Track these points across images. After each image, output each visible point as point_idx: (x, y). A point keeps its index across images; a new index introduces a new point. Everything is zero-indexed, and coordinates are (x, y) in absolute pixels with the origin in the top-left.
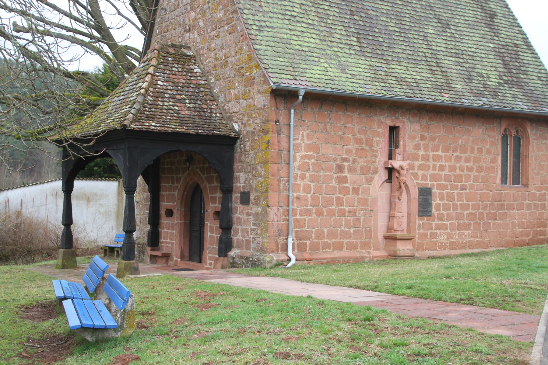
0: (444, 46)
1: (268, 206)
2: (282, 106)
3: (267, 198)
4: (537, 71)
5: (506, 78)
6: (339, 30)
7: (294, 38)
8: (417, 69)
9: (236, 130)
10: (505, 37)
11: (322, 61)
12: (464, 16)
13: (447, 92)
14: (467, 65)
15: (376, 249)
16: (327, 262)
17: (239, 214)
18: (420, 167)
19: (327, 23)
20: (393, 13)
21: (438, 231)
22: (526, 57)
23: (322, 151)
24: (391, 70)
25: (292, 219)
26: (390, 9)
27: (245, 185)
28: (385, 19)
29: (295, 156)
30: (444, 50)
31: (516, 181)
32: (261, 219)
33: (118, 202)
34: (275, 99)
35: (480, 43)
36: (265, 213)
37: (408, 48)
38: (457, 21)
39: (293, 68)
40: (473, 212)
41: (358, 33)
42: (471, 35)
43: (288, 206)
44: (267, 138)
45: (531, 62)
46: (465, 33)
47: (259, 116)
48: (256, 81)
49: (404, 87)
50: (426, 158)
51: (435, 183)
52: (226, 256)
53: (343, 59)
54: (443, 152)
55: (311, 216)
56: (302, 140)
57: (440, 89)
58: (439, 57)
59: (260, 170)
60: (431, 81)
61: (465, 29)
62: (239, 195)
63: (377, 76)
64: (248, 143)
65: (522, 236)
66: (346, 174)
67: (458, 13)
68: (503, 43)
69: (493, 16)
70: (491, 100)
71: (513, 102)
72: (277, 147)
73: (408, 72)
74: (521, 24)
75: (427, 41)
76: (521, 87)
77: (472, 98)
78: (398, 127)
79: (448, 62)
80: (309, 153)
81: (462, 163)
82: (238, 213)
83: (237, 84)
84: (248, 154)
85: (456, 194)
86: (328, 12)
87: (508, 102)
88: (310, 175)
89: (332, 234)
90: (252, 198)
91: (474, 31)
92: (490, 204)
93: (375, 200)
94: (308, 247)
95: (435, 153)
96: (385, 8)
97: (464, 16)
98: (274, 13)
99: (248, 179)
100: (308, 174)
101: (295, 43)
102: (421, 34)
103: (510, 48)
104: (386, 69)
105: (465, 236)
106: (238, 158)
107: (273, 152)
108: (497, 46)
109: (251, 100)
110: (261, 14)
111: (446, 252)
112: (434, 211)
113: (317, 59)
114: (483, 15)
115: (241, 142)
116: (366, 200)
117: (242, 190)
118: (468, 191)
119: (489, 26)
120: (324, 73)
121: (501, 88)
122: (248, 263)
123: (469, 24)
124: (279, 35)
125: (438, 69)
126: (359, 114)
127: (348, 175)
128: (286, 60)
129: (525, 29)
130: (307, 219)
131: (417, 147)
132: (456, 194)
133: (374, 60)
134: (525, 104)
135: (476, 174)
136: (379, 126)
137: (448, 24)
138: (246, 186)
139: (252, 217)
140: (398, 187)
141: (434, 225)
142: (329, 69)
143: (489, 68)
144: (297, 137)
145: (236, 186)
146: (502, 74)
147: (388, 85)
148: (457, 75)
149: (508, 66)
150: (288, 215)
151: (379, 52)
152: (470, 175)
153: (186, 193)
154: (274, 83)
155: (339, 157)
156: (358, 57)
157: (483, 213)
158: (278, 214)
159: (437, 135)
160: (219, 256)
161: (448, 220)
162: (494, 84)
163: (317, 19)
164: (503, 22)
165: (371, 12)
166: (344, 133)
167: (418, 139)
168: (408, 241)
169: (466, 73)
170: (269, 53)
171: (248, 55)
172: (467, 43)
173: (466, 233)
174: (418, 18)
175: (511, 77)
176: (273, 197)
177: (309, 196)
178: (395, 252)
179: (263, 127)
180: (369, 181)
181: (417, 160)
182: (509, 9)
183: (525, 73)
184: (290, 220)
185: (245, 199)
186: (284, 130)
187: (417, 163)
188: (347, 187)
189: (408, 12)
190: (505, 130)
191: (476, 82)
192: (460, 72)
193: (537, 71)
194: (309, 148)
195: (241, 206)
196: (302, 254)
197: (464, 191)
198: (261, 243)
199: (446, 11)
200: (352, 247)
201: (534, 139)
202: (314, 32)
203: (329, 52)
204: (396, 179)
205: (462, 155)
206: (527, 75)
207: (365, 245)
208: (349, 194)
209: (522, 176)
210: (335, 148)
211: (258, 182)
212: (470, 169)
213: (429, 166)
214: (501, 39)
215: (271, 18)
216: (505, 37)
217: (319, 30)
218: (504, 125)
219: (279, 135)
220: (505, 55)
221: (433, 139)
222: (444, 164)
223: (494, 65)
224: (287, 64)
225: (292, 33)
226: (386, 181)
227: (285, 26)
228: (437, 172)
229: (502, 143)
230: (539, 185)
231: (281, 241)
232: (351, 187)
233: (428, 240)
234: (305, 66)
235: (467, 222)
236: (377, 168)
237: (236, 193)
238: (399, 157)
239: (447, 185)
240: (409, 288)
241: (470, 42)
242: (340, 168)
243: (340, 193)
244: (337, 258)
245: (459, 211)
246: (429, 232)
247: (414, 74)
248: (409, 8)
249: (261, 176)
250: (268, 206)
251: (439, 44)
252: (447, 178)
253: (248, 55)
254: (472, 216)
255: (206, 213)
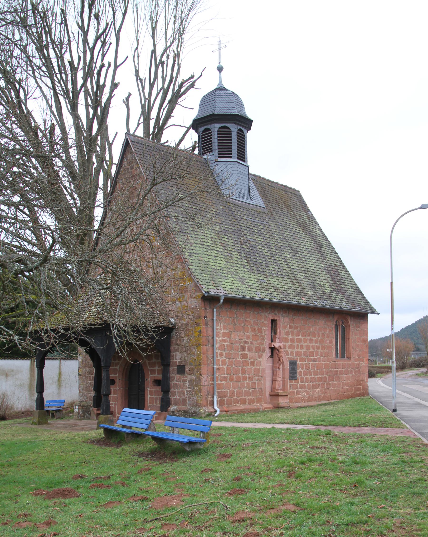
0: (297, 265)
1: (201, 375)
2: (208, 307)
3: (200, 369)
4: (350, 283)
5: (334, 287)
6: (236, 255)
7: (211, 260)
8: (284, 281)
9: (172, 323)
10: (330, 260)
11: (229, 276)
12: (305, 246)
13: (304, 297)
14: (312, 279)
15: (265, 403)
16: (238, 412)
17: (176, 381)
18: (290, 347)
19: (228, 250)
20: (265, 243)
21: (301, 390)
22: (343, 273)
23: (232, 337)
24: (269, 282)
25: (215, 383)
26: (262, 240)
27: (181, 361)
28: (261, 247)
29: (216, 340)
30: (297, 268)
31: (343, 355)
32: (196, 384)
33: (31, 376)
34: (204, 303)
35: (317, 264)
36: (199, 380)
37: (277, 267)
38: (301, 249)
39: (214, 281)
40: (321, 376)
41: (247, 257)
42: (311, 258)
43: (213, 374)
44: (199, 329)
45: (346, 277)
46: (307, 257)
47: (192, 314)
48: (189, 290)
49: (279, 293)
50: (292, 341)
51: (298, 357)
52: (166, 411)
53: (241, 275)
54: (302, 336)
55: (227, 381)
56: (221, 329)
57: (300, 294)
58: (295, 273)
59: (194, 350)
60: (293, 289)
61: (307, 254)
62: (176, 368)
63: (263, 286)
64: (183, 332)
65: (348, 392)
66: (247, 352)
67: (302, 244)
68: (329, 264)
69: (321, 246)
70: (329, 302)
71: (341, 304)
72: (205, 335)
73: (279, 283)
74: (337, 252)
75: (287, 262)
76: (343, 293)
77: (318, 301)
78: (276, 320)
79: (300, 276)
80: (224, 338)
81: (314, 344)
82: (175, 380)
83: (172, 291)
84: (184, 339)
85: (310, 364)
86: (228, 243)
87: (338, 303)
88: (225, 353)
89: (239, 393)
90: (187, 369)
91: (312, 256)
92: (330, 371)
93: (264, 370)
94: (226, 402)
95: (298, 337)
96: (260, 240)
97: (305, 246)
98: (197, 244)
99: (184, 357)
100: (224, 353)
101: (212, 264)
102: (283, 258)
103: (333, 267)
104: (266, 281)
105: (317, 393)
106: (174, 342)
107: (203, 338)
108: (326, 266)
109: (185, 302)
110: (189, 245)
111: (306, 404)
112: (298, 376)
113: (226, 275)
114: (315, 245)
115: (176, 331)
116: (259, 369)
117: (178, 364)
118: (317, 362)
119: (320, 252)
120: (232, 284)
121: (333, 294)
122: (186, 414)
123: (308, 251)
124: (202, 259)
125: (296, 281)
126: (253, 312)
127: (248, 353)
128: (209, 276)
129: (339, 255)
130: (224, 383)
131: (287, 333)
132: (310, 364)
133: (259, 275)
134: (348, 305)
135: (321, 351)
136: (265, 320)
137: (297, 251)
138: (182, 362)
139: (187, 383)
140: (278, 360)
141: (298, 386)
142: (234, 281)
143: (324, 281)
144: (217, 327)
145: (173, 362)
146: (331, 285)
147: (270, 292)
148: (307, 286)
149: (334, 280)
150: (213, 381)
151: (261, 270)
152: (318, 352)
153: (126, 367)
154: (206, 292)
155: (242, 341)
156: (250, 274)
157: (326, 377)
158: (207, 380)
159: (298, 325)
160: (161, 411)
161: (306, 382)
162: (328, 291)
163: (222, 247)
164: (327, 250)
165: (252, 243)
166: (245, 325)
167: (287, 328)
168: (286, 397)
169: (312, 284)
170: (198, 271)
171: (182, 272)
172: (310, 264)
173: (317, 390)
174: (279, 247)
175: (337, 286)
176: (204, 369)
177: (225, 367)
178: (279, 404)
179: (195, 321)
180: (260, 356)
181: (287, 342)
182: (329, 241)
183: (344, 284)
184: (215, 384)
185: (181, 370)
186: (210, 323)
187: (287, 344)
188: (247, 361)
189: (273, 243)
190: (336, 322)
191: (318, 290)
192: (308, 283)
193: (350, 283)
194: (225, 335)
195: (178, 375)
196: (222, 407)
197: (315, 363)
198: (195, 401)
199: (294, 242)
200: (251, 402)
201: (352, 328)
202: (222, 256)
203: (232, 270)
204: (277, 355)
205: (313, 338)
206: (345, 285)
207: (259, 401)
208: (249, 366)
209: (347, 352)
210: (240, 334)
211: (193, 358)
212: (318, 348)
213: (294, 346)
214: (328, 261)
215: (195, 247)
216: (330, 260)
217: (225, 255)
218: (336, 318)
219: (207, 326)
220: (332, 272)
221: (296, 328)
222: (303, 344)
223: (326, 278)
224: (210, 278)
225: (209, 257)
226: (270, 357)
227: (204, 253)
228: (299, 350)
229: (335, 330)
230: (356, 357)
231: (209, 398)
232: (249, 361)
233: (295, 396)
234: (220, 280)
235: (317, 383)
236: (265, 348)
237: (173, 366)
238: (278, 340)
239: (305, 359)
240: (323, 421)
241: (311, 263)
242: (243, 348)
243: (243, 365)
244: (243, 409)
245: (313, 376)
246: (296, 391)
247: (283, 284)
248: (274, 240)
249: (195, 354)
250: (201, 375)
251: (294, 264)
252: (305, 353)
253: (182, 272)
254: (320, 379)
255: (146, 381)
